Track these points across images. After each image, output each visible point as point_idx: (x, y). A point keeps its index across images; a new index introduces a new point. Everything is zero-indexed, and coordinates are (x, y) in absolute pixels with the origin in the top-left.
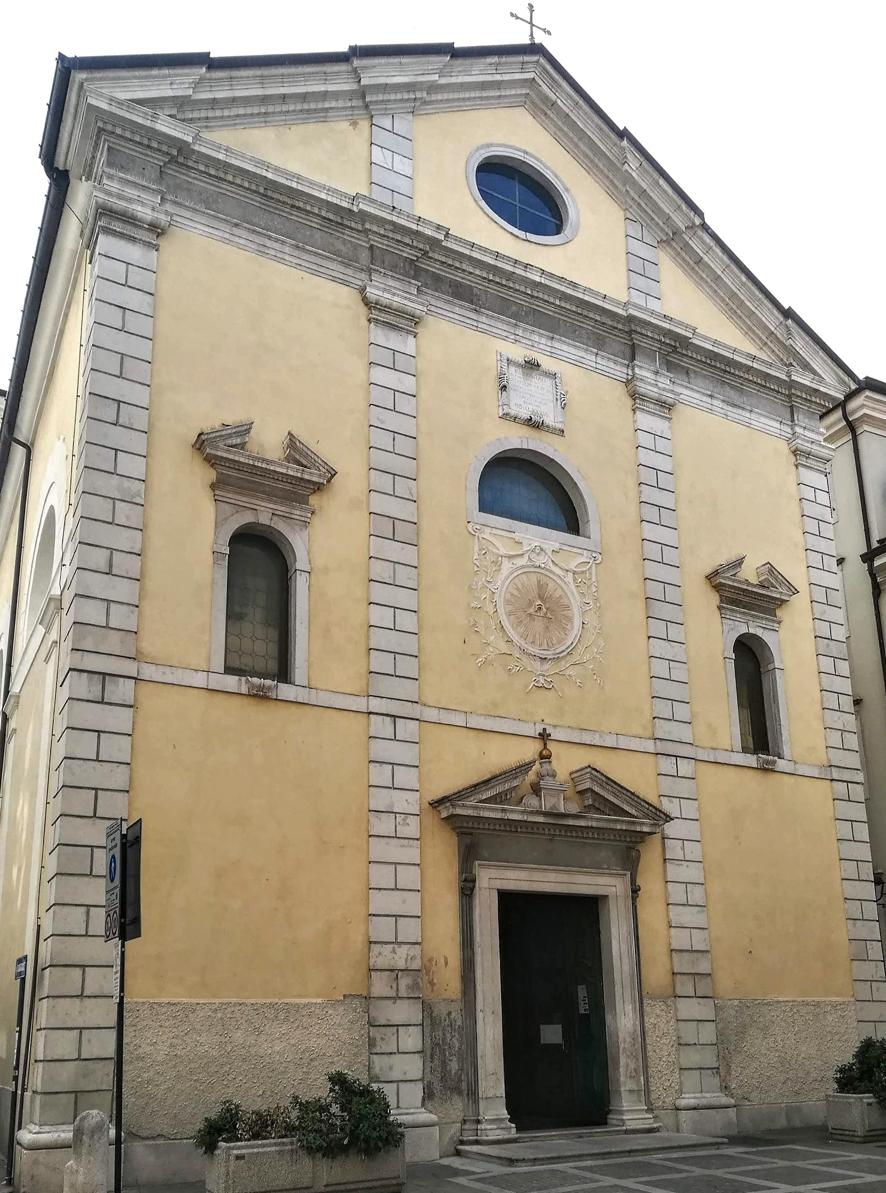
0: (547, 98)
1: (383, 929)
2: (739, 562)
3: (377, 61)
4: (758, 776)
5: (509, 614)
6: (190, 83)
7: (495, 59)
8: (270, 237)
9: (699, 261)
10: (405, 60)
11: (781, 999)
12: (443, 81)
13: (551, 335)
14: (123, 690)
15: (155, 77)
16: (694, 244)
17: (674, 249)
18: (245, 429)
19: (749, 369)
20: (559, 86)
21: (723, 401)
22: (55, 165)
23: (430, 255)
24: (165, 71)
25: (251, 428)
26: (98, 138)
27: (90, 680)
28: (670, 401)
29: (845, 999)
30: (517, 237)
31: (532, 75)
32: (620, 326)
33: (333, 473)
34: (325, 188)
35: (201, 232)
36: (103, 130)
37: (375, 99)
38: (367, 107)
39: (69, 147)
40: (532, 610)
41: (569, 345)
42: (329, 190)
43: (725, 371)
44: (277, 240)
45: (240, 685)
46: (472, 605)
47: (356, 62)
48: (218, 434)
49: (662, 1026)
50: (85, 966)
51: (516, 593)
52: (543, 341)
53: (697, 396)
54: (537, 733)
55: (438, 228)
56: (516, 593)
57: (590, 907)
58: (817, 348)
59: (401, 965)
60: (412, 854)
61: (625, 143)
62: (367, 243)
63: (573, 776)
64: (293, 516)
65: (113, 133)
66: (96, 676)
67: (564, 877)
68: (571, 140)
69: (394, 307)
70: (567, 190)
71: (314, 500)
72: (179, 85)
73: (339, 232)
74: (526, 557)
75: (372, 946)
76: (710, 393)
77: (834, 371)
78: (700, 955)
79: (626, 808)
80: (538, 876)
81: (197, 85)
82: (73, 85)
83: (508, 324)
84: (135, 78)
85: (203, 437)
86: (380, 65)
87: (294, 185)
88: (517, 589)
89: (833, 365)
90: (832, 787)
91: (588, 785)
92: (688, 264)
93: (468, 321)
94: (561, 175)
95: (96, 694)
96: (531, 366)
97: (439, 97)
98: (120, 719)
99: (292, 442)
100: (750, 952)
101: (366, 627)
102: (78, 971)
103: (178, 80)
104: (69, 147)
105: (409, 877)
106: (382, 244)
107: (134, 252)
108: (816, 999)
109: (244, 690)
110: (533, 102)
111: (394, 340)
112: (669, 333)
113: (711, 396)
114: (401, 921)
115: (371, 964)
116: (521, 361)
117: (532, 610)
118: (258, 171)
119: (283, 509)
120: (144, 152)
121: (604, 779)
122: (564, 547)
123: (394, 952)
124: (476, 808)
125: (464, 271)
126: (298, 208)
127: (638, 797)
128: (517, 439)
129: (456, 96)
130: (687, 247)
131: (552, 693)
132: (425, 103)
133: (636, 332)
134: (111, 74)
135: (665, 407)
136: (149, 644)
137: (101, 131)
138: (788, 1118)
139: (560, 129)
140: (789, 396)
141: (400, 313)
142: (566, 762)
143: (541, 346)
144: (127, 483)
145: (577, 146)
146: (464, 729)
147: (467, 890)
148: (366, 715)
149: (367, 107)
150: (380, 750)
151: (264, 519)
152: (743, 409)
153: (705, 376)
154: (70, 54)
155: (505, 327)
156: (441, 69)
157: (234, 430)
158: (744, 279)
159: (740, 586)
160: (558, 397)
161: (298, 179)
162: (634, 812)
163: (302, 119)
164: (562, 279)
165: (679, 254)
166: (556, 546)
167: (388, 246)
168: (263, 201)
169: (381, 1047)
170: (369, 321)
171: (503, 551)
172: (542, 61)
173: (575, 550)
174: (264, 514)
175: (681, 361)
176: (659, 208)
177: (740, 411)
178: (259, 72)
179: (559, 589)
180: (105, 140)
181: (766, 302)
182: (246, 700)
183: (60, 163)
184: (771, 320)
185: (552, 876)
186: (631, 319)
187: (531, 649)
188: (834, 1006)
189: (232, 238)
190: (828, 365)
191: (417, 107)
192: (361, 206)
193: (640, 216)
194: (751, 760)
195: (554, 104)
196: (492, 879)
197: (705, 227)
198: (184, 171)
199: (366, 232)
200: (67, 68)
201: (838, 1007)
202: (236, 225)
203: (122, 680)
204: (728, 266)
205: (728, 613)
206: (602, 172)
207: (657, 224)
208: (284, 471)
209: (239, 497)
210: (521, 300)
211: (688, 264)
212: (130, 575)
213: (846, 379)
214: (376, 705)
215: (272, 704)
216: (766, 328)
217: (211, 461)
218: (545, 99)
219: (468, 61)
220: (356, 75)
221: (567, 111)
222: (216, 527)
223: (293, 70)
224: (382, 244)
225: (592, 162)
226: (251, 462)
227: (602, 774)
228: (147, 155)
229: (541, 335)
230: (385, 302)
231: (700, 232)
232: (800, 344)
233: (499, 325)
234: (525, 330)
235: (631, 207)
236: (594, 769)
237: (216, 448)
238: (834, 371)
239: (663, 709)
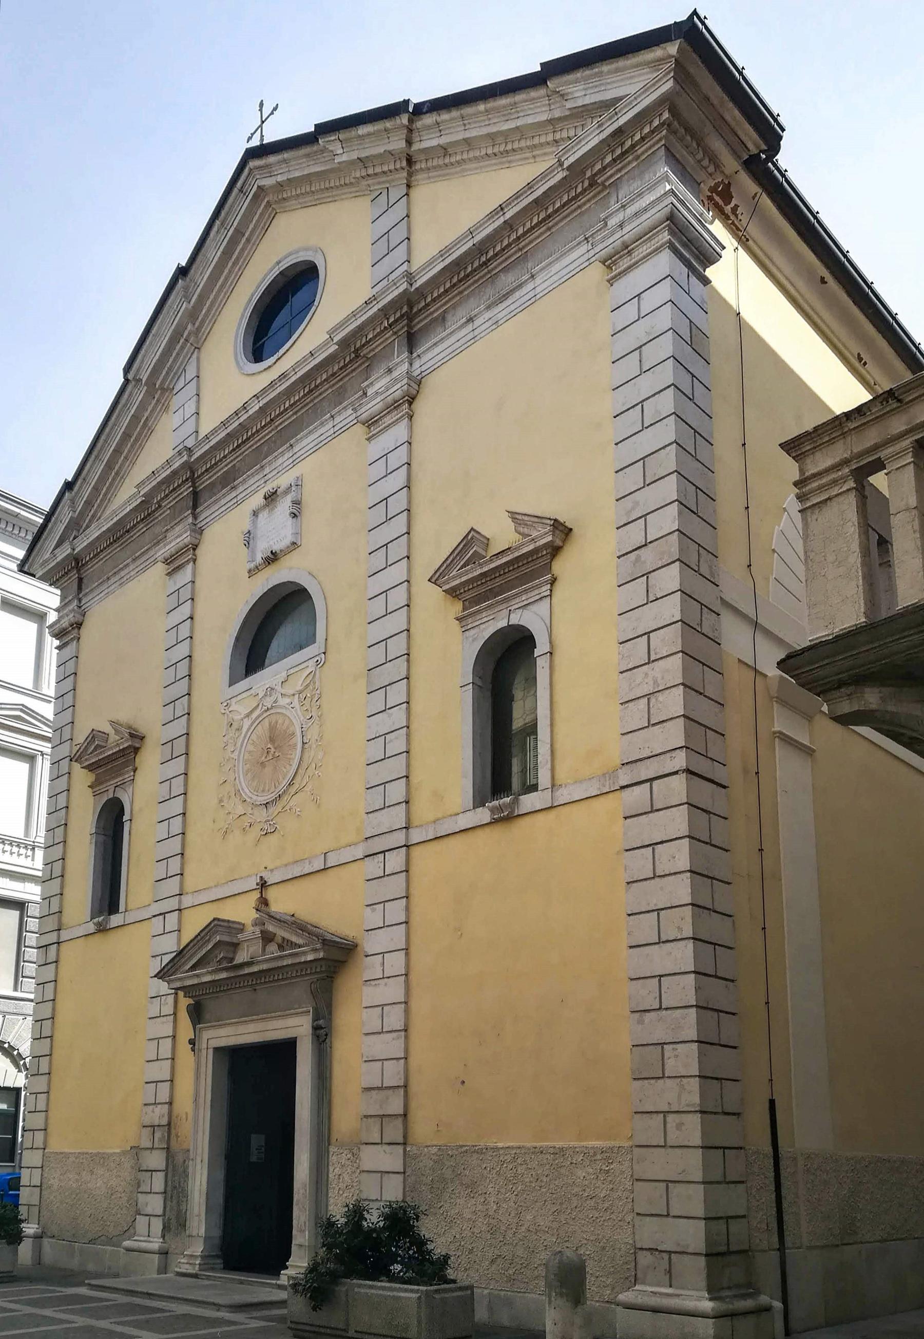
4: (497, 832)
8: (122, 569)
11: (500, 1145)
13: (288, 445)
15: (52, 528)
19: (509, 225)
21: (488, 308)
29: (617, 1144)
30: (270, 367)
41: (306, 436)
43: (485, 263)
49: (347, 1178)
53: (453, 339)
57: (282, 1053)
67: (260, 1026)
76: (464, 320)
77: (637, 66)
78: (390, 1092)
80: (242, 1029)
100: (463, 1082)
108: (559, 1144)
112: (385, 312)
114: (662, 913)
116: (262, 501)
122: (292, 671)
131: (276, 835)
132: (198, 330)
138: (490, 1309)
152: (520, 286)
153: (454, 307)
155: (256, 478)
156: (184, 296)
159: (470, 576)
169: (145, 1188)
175: (432, 313)
177: (517, 294)
185: (252, 1027)
188: (590, 1155)
194: (483, 815)
197: (421, 109)
201: (599, 1157)
202: (108, 578)
205: (470, 620)
216: (540, 125)
233: (251, 481)
238: (637, 66)
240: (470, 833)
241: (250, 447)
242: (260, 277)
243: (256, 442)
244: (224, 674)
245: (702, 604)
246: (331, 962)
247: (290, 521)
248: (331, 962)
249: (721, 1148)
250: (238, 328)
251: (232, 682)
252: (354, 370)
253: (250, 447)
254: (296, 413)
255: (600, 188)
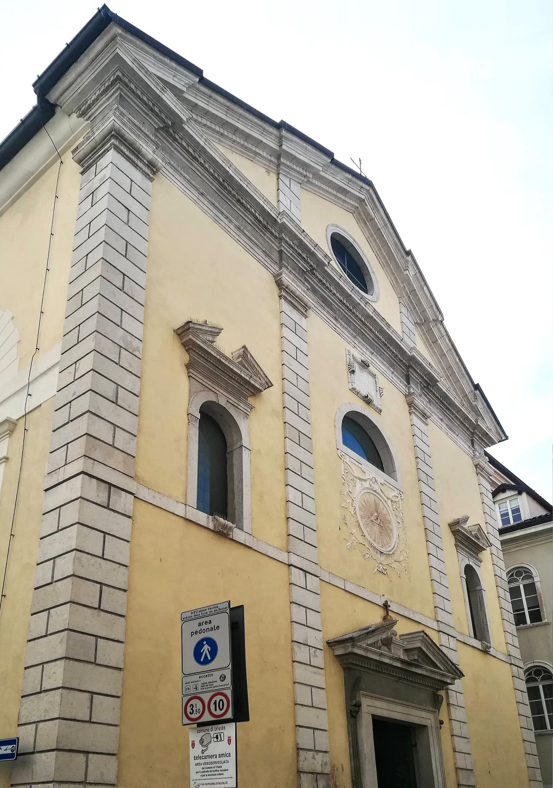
0: (369, 214)
1: (306, 739)
2: (466, 519)
3: (295, 138)
4: (479, 654)
5: (362, 517)
6: (186, 83)
7: (350, 176)
9: (435, 342)
10: (309, 148)
12: (322, 173)
13: (373, 351)
14: (123, 502)
15: (165, 64)
16: (435, 330)
17: (422, 330)
18: (216, 332)
20: (378, 210)
22: (47, 97)
23: (314, 272)
24: (174, 64)
25: (220, 333)
26: (113, 84)
27: (98, 486)
28: (428, 414)
31: (363, 197)
32: (404, 361)
33: (270, 385)
34: (263, 198)
35: (178, 187)
36: (121, 80)
37: (285, 162)
38: (278, 166)
39: (70, 85)
40: (373, 518)
42: (265, 201)
44: (227, 218)
45: (208, 522)
46: (342, 505)
47: (284, 133)
48: (200, 327)
50: (88, 753)
51: (364, 504)
52: (368, 353)
54: (382, 603)
55: (325, 256)
56: (364, 504)
58: (489, 411)
59: (319, 769)
60: (318, 679)
61: (409, 258)
62: (278, 248)
63: (402, 638)
64: (239, 407)
65: (127, 86)
66: (104, 485)
68: (378, 246)
69: (296, 295)
70: (373, 272)
71: (251, 400)
72: (182, 80)
73: (263, 232)
74: (368, 482)
75: (301, 752)
79: (438, 664)
81: (191, 87)
82: (101, 39)
83: (351, 334)
84: (153, 56)
85: (191, 325)
86: (295, 142)
87: (245, 186)
88: (364, 501)
89: (495, 423)
90: (512, 669)
91: (418, 645)
92: (428, 341)
93: (330, 323)
94: (371, 263)
95: (102, 498)
96: (365, 365)
97: (317, 183)
98: (119, 525)
99: (245, 352)
101: (284, 502)
102: (81, 758)
103: (180, 76)
104: (70, 85)
105: (320, 698)
106: (289, 252)
107: (137, 176)
109: (211, 526)
110: (359, 213)
111: (295, 315)
113: (442, 420)
115: (300, 766)
117: (373, 518)
118: (224, 165)
119: (234, 400)
120: (146, 111)
121: (430, 642)
123: (314, 758)
124: (366, 650)
125: (331, 291)
126: (242, 204)
127: (447, 658)
128: (360, 407)
129: (324, 187)
130: (430, 330)
133: (412, 367)
134: (139, 42)
135: (425, 416)
136: (142, 470)
137: (118, 79)
139: (372, 236)
140: (473, 434)
141: (299, 300)
142: (402, 628)
143: (366, 355)
144: (129, 338)
145: (380, 250)
146: (343, 591)
147: (353, 712)
148: (287, 566)
149: (278, 166)
150: (299, 595)
151: (222, 402)
154: (114, 9)
157: (210, 329)
158: (458, 360)
160: (378, 390)
161: (248, 183)
162: (442, 668)
163: (241, 151)
164: (383, 319)
165: (424, 334)
166: (383, 481)
167: (291, 254)
168: (219, 188)
170: (280, 297)
171: (356, 475)
172: (371, 191)
173: (391, 486)
174: (223, 399)
176: (420, 303)
178: (228, 104)
179: (385, 509)
180: (119, 88)
181: (467, 377)
182: (211, 535)
183: (52, 97)
184: (468, 389)
185: (400, 708)
186: (413, 358)
187: (375, 545)
189: (197, 200)
190: (493, 422)
191: (305, 182)
192: (284, 220)
193: (408, 304)
195: (372, 219)
196: (372, 706)
198: (171, 141)
199: (281, 239)
200: (104, 19)
202: (202, 194)
203: (123, 493)
204: (450, 350)
206: (391, 270)
207: (417, 312)
208: (239, 372)
209: (205, 380)
210: (357, 324)
211: (428, 341)
212: (131, 410)
213: (501, 432)
214: (294, 560)
215: (228, 541)
217: (189, 346)
218: (368, 214)
219: (338, 170)
220: (280, 140)
221: (380, 227)
222: (190, 396)
223: (247, 115)
224: (289, 252)
225: (387, 262)
226: (218, 357)
227: (430, 639)
228: (147, 115)
229: (367, 349)
230: (292, 288)
231: (439, 325)
232: (480, 406)
234: (359, 342)
235: (404, 297)
236: (426, 634)
237: (198, 337)
239: (299, 614)
240: (353, 596)
241: (345, 312)
242: (374, 270)
243: (350, 317)
244: (379, 713)
245: (298, 415)
246: (461, 675)
247: (364, 393)
248: (461, 675)
249: (312, 728)
250: (348, 234)
251: (372, 715)
252: (400, 366)
253: (345, 312)
254: (373, 339)
255: (278, 245)
